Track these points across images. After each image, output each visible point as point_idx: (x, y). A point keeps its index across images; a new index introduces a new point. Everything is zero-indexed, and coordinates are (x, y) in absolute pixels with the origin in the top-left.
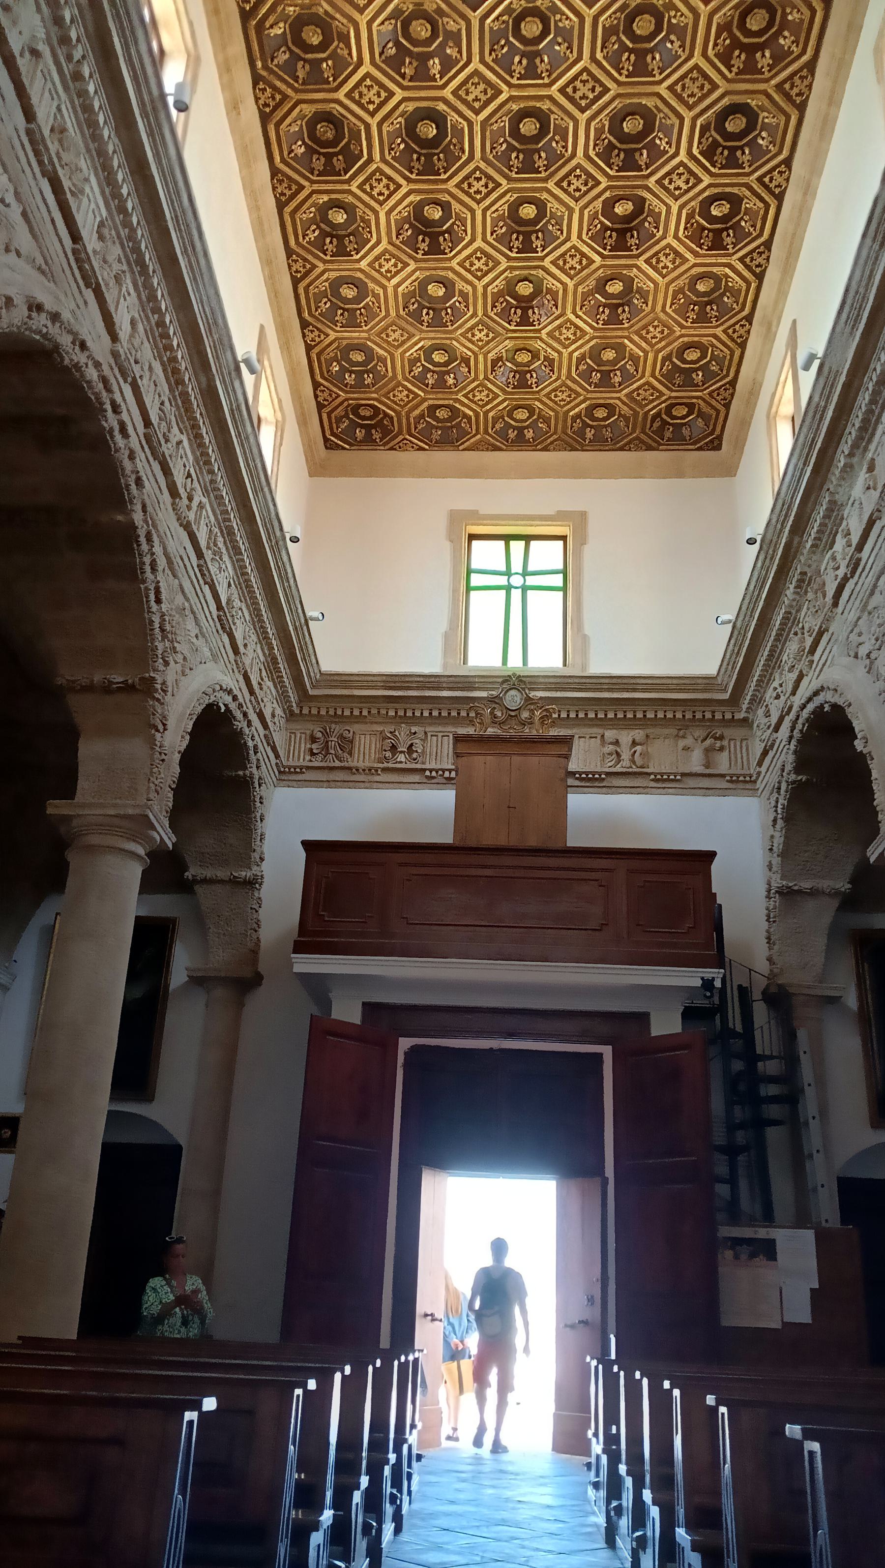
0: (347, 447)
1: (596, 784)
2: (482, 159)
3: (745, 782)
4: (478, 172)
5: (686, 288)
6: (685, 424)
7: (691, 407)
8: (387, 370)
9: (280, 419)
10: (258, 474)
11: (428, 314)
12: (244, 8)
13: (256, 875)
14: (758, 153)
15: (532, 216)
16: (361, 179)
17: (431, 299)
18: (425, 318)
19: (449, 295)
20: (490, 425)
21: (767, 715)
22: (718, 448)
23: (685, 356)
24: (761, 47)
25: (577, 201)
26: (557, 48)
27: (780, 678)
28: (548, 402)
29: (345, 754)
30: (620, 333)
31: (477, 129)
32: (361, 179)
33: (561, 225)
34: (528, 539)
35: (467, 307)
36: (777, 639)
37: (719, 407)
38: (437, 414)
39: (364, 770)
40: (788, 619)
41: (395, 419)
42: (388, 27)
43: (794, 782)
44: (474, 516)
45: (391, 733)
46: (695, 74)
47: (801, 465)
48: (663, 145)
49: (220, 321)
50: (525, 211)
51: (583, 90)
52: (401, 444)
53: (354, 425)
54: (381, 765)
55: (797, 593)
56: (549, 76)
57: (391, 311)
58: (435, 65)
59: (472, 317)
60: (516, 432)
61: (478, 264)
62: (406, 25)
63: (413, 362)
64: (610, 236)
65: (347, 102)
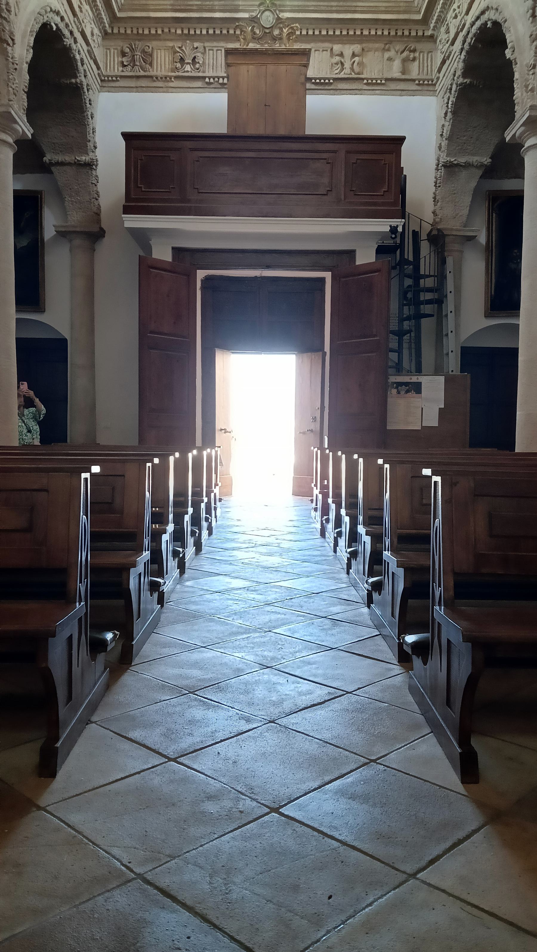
3: (428, 85)
29: (148, 66)
39: (161, 78)
43: (461, 84)
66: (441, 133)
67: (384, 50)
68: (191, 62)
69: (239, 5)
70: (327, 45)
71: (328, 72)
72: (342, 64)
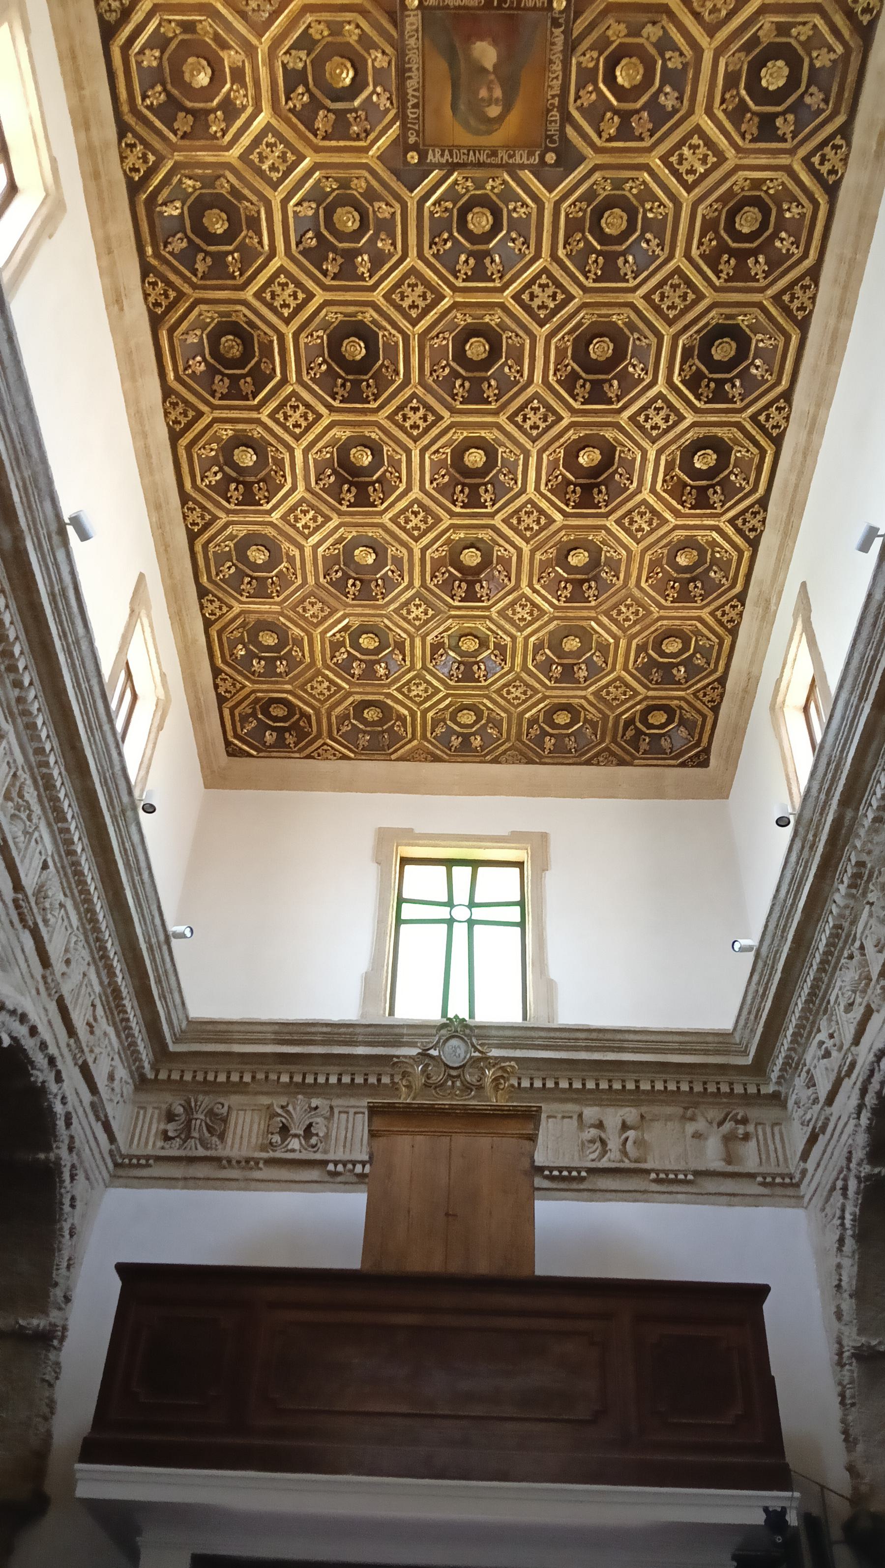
0: (255, 753)
1: (574, 1186)
2: (420, 383)
3: (783, 1185)
4: (415, 401)
5: (664, 561)
6: (663, 735)
7: (669, 711)
8: (303, 655)
9: (162, 697)
10: (94, 702)
11: (354, 585)
12: (132, 178)
13: (55, 1325)
14: (750, 384)
15: (480, 465)
16: (273, 405)
17: (360, 568)
18: (352, 590)
19: (380, 563)
20: (429, 728)
21: (811, 1083)
22: (705, 764)
23: (664, 647)
24: (754, 253)
25: (534, 442)
26: (511, 244)
27: (829, 1026)
28: (499, 700)
29: (215, 1139)
30: (585, 613)
31: (415, 344)
32: (273, 405)
33: (515, 474)
34: (475, 864)
35: (401, 576)
36: (822, 969)
37: (706, 711)
38: (365, 715)
39: (238, 1162)
40: (838, 936)
41: (313, 718)
42: (308, 210)
43: (869, 1177)
44: (409, 836)
45: (282, 1107)
46: (676, 280)
47: (854, 700)
48: (637, 372)
49: (34, 451)
50: (472, 458)
51: (542, 297)
52: (320, 751)
54: (264, 1155)
55: (853, 896)
56: (501, 278)
57: (309, 580)
58: (363, 262)
59: (407, 588)
60: (460, 739)
61: (415, 521)
62: (329, 213)
63: (336, 646)
64: (574, 492)
65: (257, 304)
66: (837, 1282)
67: (684, 1118)
68: (302, 1133)
69: (402, 1035)
70: (571, 1107)
71: (576, 1157)
72: (603, 1142)
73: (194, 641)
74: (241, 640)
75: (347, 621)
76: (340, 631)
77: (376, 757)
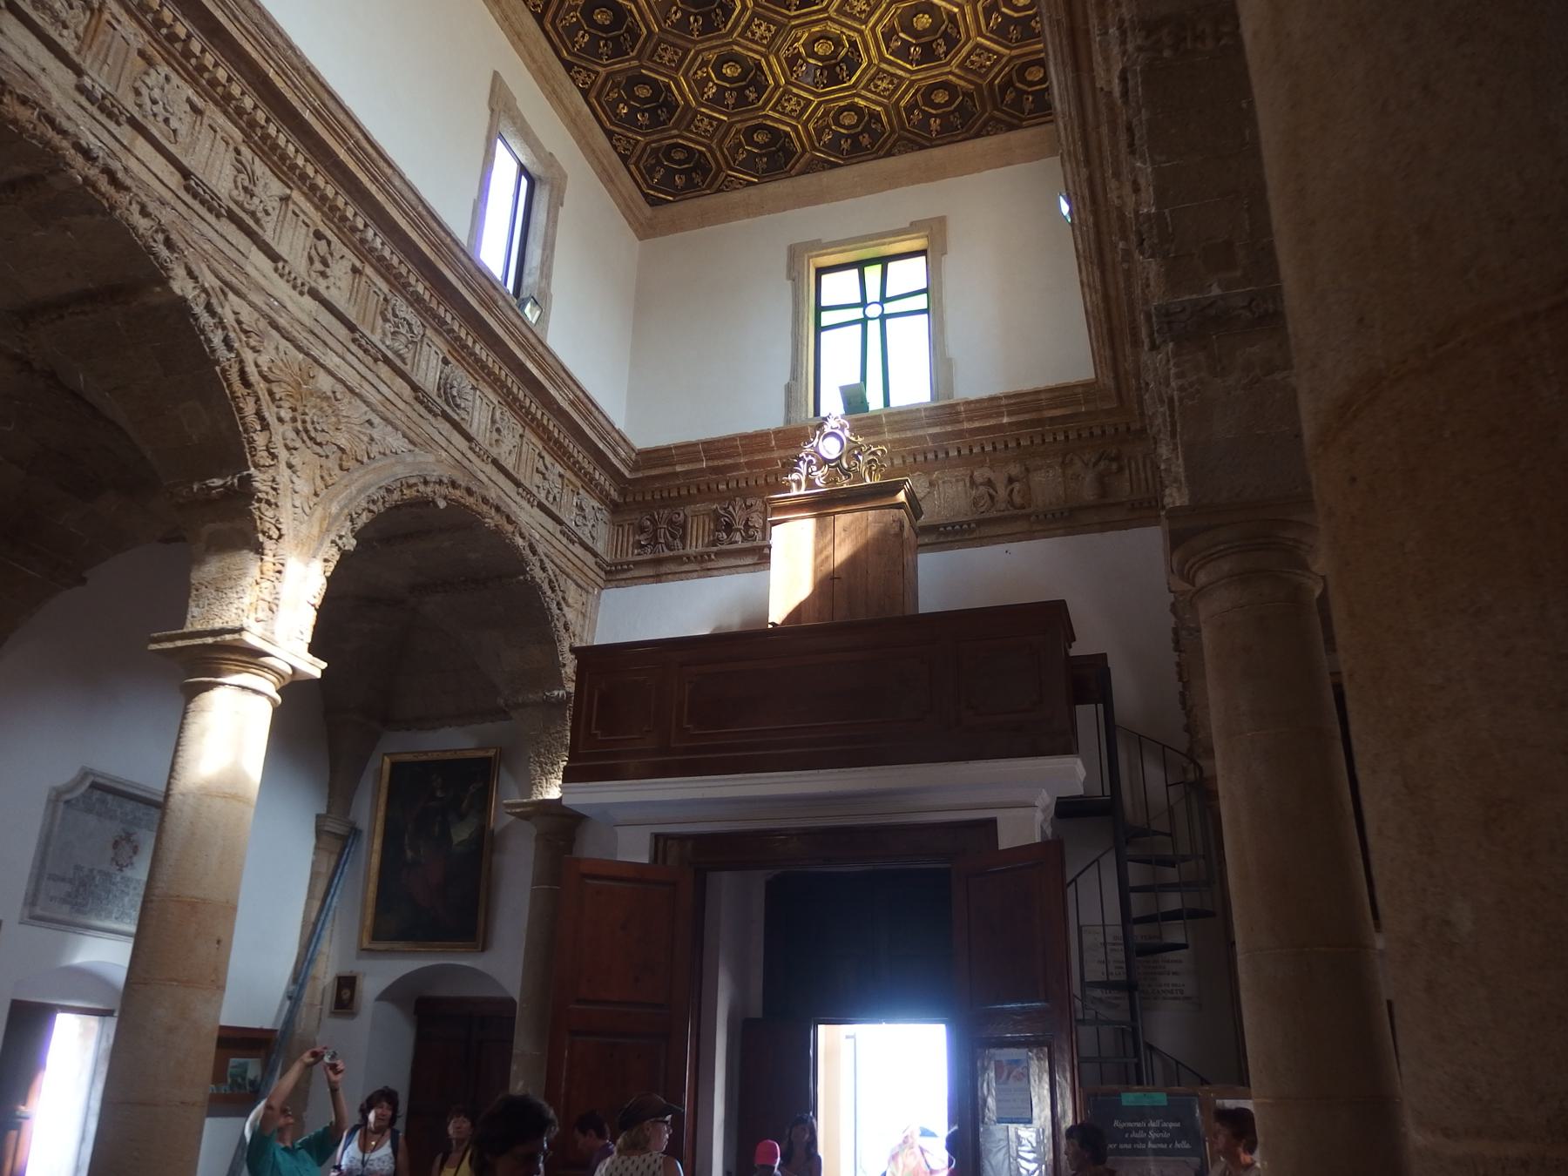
0: (671, 198)
1: (967, 537)
28: (869, 95)
39: (695, 557)
44: (556, 203)
45: (725, 509)
52: (726, 183)
53: (670, 173)
54: (715, 549)
73: (579, 113)
74: (620, 99)
75: (700, 57)
76: (700, 68)
77: (778, 177)
